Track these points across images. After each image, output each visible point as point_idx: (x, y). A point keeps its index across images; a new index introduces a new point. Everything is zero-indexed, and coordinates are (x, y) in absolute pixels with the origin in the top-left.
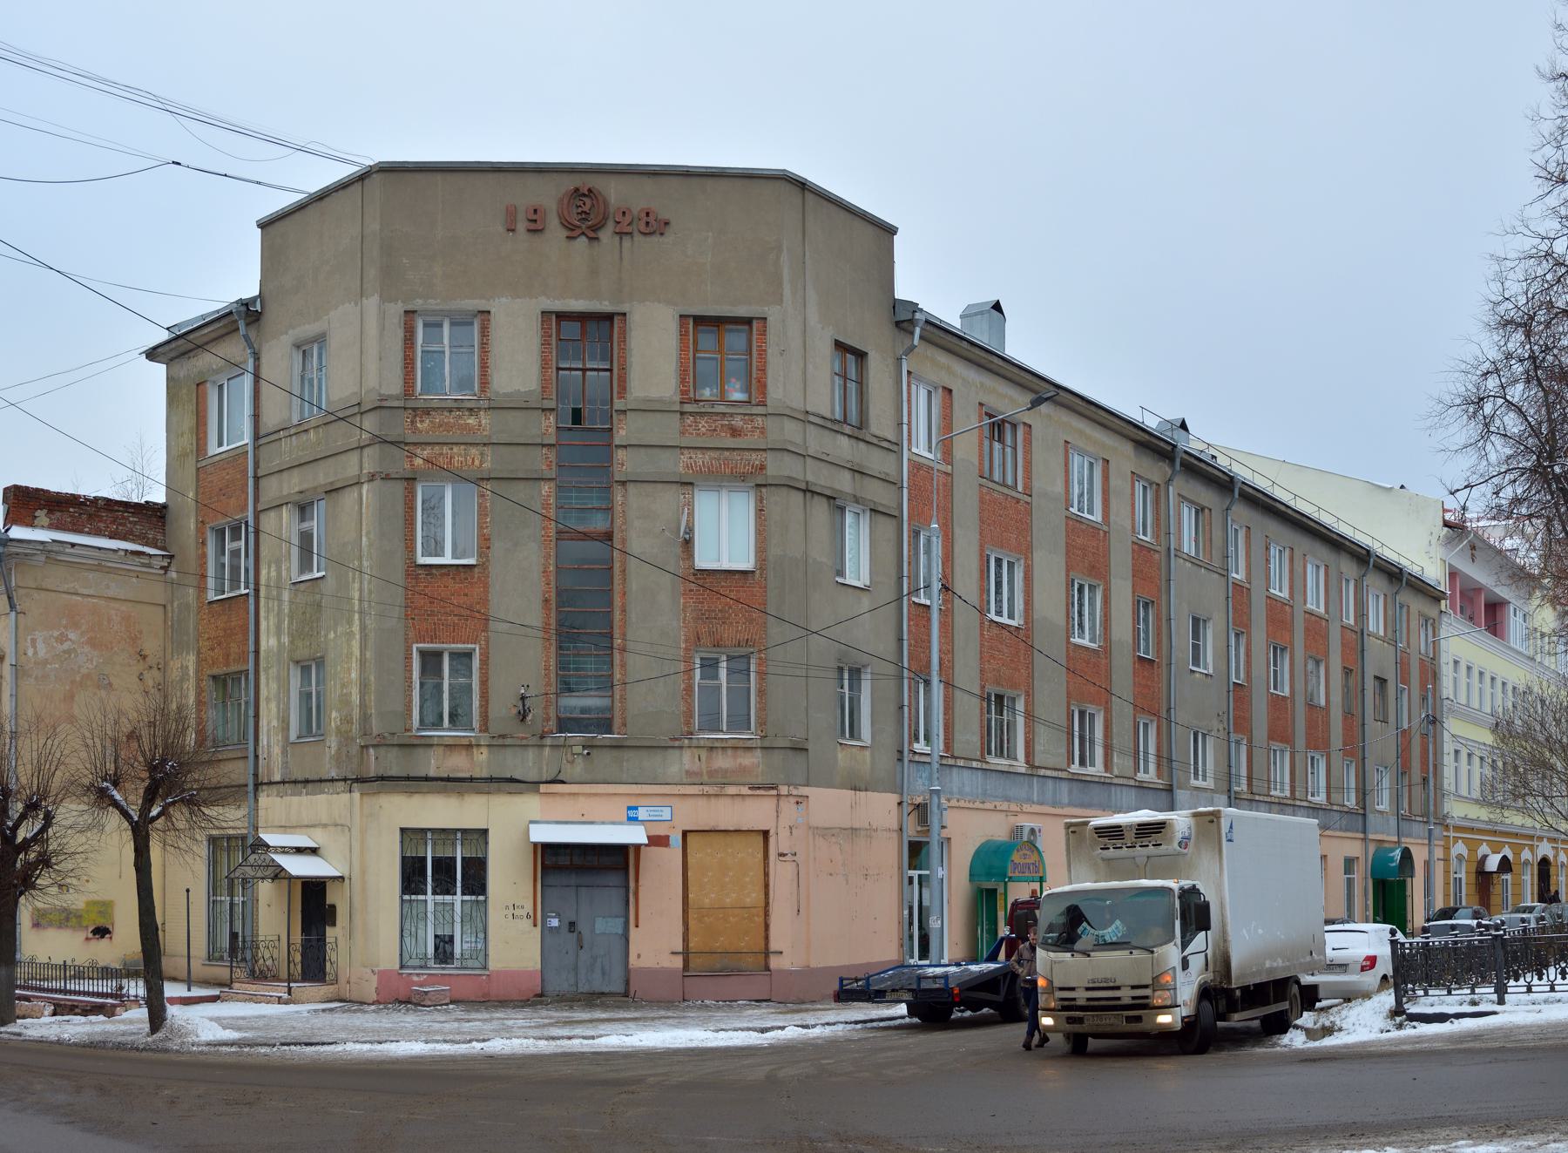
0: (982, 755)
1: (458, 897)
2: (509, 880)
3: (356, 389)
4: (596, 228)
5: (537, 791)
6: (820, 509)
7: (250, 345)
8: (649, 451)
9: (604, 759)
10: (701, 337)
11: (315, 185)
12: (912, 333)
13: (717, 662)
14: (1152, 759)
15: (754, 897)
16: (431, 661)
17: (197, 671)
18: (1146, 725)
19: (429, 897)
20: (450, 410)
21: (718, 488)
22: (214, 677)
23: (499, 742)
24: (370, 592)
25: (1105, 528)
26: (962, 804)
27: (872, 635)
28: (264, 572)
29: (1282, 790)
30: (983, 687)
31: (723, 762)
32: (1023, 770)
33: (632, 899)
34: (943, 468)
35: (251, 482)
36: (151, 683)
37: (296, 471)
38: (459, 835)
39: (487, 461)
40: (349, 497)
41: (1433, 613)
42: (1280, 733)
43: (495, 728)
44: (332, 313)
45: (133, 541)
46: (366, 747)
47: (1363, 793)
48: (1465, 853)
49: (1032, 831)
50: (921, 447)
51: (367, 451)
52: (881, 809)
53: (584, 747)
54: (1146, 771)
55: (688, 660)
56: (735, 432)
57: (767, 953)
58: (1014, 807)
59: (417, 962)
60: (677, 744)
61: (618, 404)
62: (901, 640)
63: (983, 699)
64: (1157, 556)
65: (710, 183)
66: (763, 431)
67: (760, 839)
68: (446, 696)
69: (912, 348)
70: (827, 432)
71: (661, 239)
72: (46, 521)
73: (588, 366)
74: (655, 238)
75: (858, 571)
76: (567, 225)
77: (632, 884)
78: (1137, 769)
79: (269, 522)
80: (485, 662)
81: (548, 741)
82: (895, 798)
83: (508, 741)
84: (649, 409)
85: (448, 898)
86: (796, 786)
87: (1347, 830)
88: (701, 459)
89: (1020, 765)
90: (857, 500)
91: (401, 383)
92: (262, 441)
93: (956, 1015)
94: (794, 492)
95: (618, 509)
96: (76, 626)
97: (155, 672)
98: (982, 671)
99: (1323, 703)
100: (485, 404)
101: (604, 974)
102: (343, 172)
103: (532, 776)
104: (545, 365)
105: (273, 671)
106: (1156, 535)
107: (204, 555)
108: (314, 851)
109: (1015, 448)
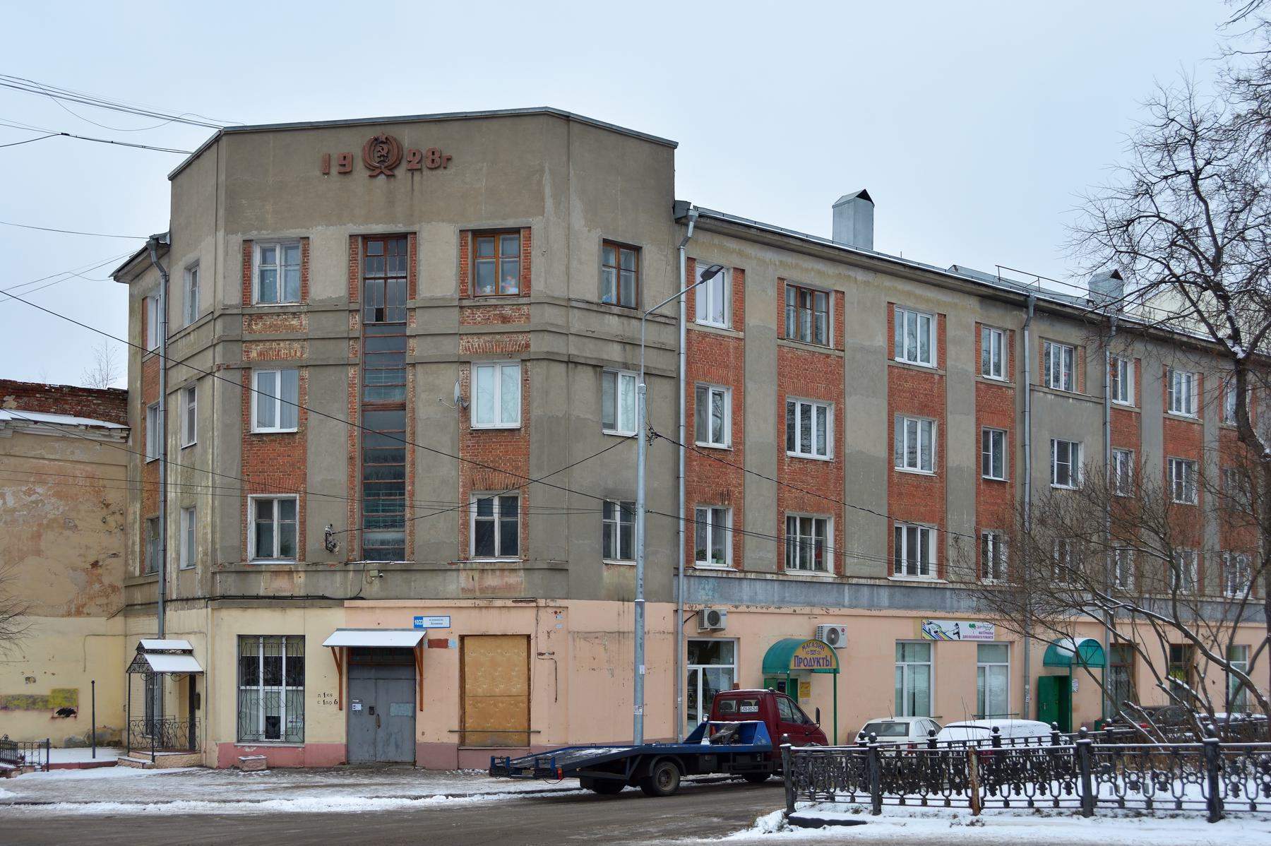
0: (780, 567)
1: (261, 687)
2: (321, 676)
5: (342, 606)
6: (585, 378)
7: (162, 270)
8: (436, 339)
9: (396, 581)
11: (194, 147)
12: (687, 225)
13: (490, 501)
15: (519, 687)
16: (264, 508)
19: (261, 687)
20: (278, 315)
21: (493, 365)
23: (313, 569)
25: (941, 372)
26: (753, 609)
27: (642, 478)
31: (492, 581)
34: (735, 334)
35: (162, 372)
36: (113, 524)
38: (261, 640)
39: (305, 352)
40: (209, 380)
43: (309, 559)
45: (97, 418)
49: (833, 631)
56: (505, 319)
57: (529, 732)
59: (251, 737)
61: (410, 304)
64: (1011, 392)
65: (485, 125)
66: (528, 317)
67: (525, 641)
71: (445, 172)
72: (14, 404)
74: (440, 172)
76: (370, 167)
77: (418, 677)
80: (303, 507)
81: (351, 567)
82: (672, 606)
83: (320, 568)
85: (275, 688)
86: (553, 599)
88: (476, 342)
89: (829, 575)
90: (626, 366)
91: (240, 295)
93: (628, 788)
94: (554, 365)
96: (44, 483)
97: (118, 517)
98: (780, 500)
100: (305, 309)
101: (397, 746)
103: (340, 594)
104: (352, 276)
106: (1011, 375)
108: (189, 652)
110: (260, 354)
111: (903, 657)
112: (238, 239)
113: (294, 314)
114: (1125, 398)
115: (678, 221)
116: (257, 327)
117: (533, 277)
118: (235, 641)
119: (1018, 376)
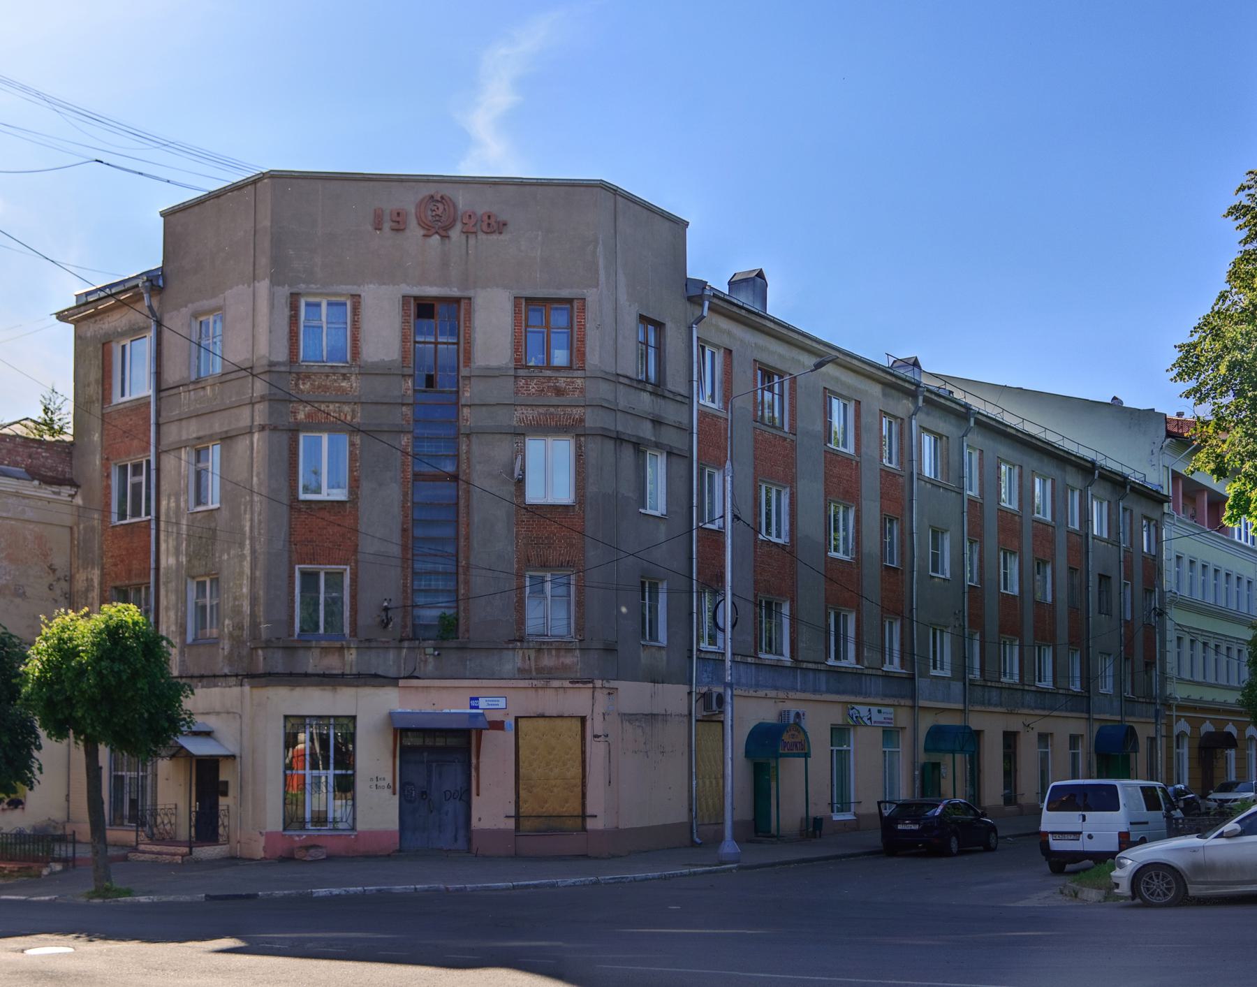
3: (249, 356)
4: (447, 228)
5: (397, 685)
10: (531, 314)
14: (896, 654)
16: (310, 579)
17: (101, 583)
18: (891, 624)
22: (116, 588)
23: (367, 644)
24: (260, 522)
28: (164, 503)
29: (1011, 677)
30: (756, 596)
32: (789, 664)
33: (474, 773)
36: (58, 592)
37: (194, 421)
41: (1156, 515)
42: (1010, 628)
44: (228, 293)
46: (256, 648)
47: (1087, 679)
48: (1188, 729)
49: (798, 715)
50: (706, 400)
51: (257, 406)
52: (673, 698)
53: (435, 649)
54: (891, 663)
55: (520, 576)
57: (584, 816)
58: (782, 695)
60: (511, 646)
62: (691, 558)
63: (756, 605)
64: (901, 480)
67: (577, 725)
68: (322, 607)
69: (702, 317)
70: (633, 391)
73: (440, 340)
74: (495, 237)
75: (657, 502)
76: (421, 224)
77: (474, 761)
78: (883, 662)
79: (169, 462)
80: (354, 580)
84: (489, 374)
86: (608, 680)
87: (1072, 711)
88: (530, 413)
89: (786, 657)
91: (286, 351)
92: (163, 394)
95: (463, 456)
99: (1049, 599)
102: (236, 177)
103: (392, 672)
104: (404, 339)
105: (172, 585)
106: (901, 463)
107: (108, 487)
109: (781, 396)
110: (309, 416)
111: (798, 715)
112: (284, 291)
113: (344, 375)
114: (942, 669)
115: (690, 299)
116: (305, 387)
117: (588, 350)
118: (353, 714)
119: (906, 465)
